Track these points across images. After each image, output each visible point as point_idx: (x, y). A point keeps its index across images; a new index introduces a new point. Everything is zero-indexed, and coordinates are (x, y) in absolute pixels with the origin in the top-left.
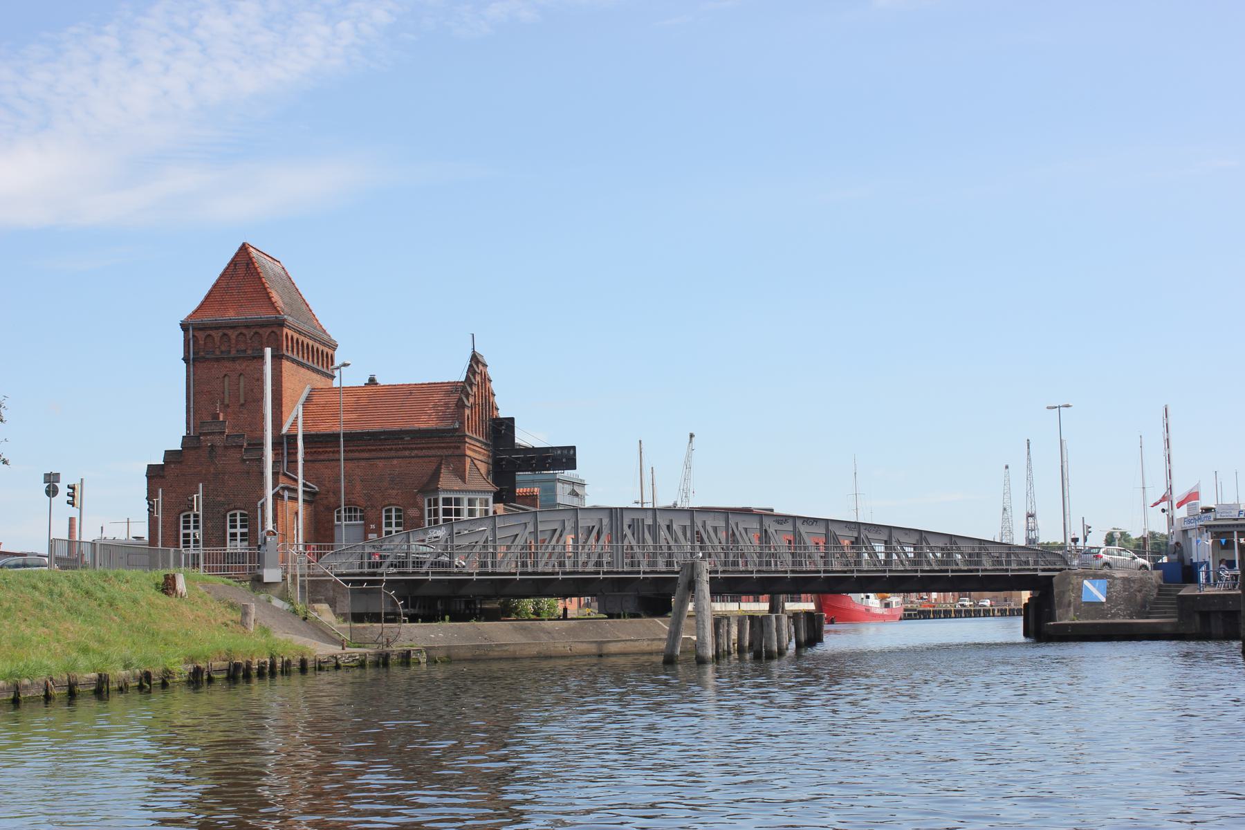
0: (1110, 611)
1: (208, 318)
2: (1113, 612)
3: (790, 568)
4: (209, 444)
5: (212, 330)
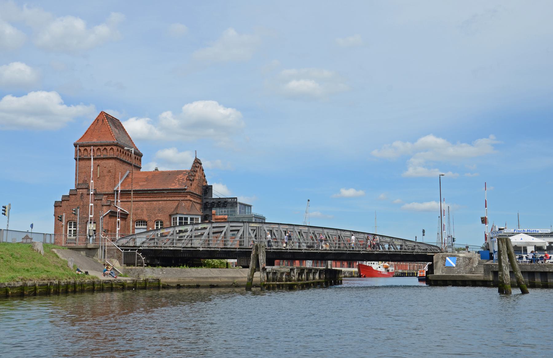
0: (457, 270)
1: (85, 142)
2: (458, 271)
3: (238, 247)
4: (81, 193)
5: (87, 147)
